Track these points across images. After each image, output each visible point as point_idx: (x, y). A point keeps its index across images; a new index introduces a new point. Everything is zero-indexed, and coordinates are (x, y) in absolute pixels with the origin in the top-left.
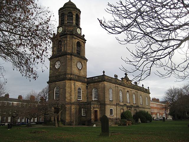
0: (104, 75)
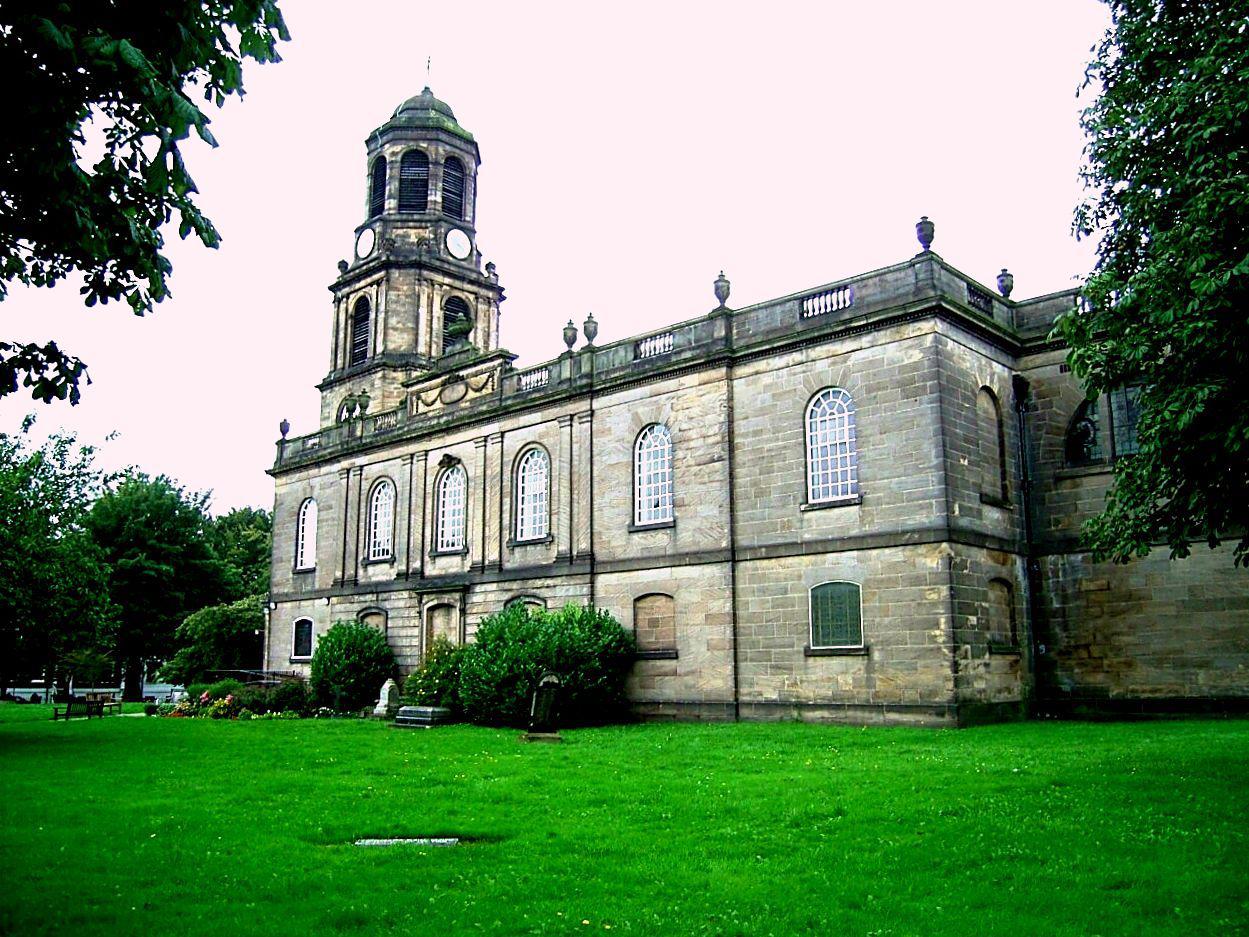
0: (725, 314)
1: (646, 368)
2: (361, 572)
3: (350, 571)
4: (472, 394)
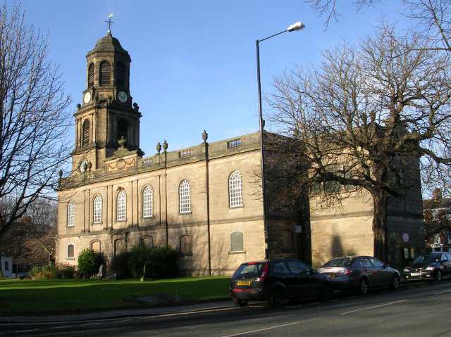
1: (183, 159)
2: (91, 227)
3: (87, 227)
4: (127, 166)
